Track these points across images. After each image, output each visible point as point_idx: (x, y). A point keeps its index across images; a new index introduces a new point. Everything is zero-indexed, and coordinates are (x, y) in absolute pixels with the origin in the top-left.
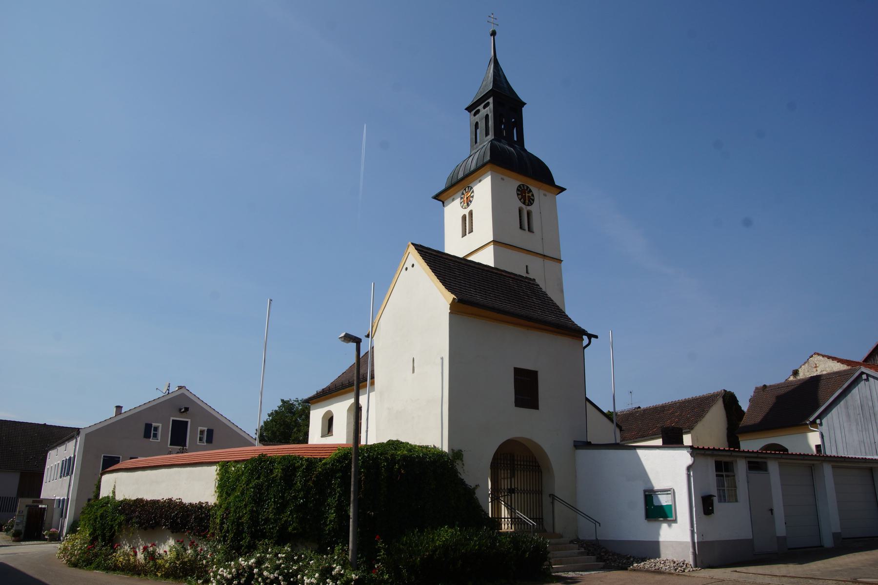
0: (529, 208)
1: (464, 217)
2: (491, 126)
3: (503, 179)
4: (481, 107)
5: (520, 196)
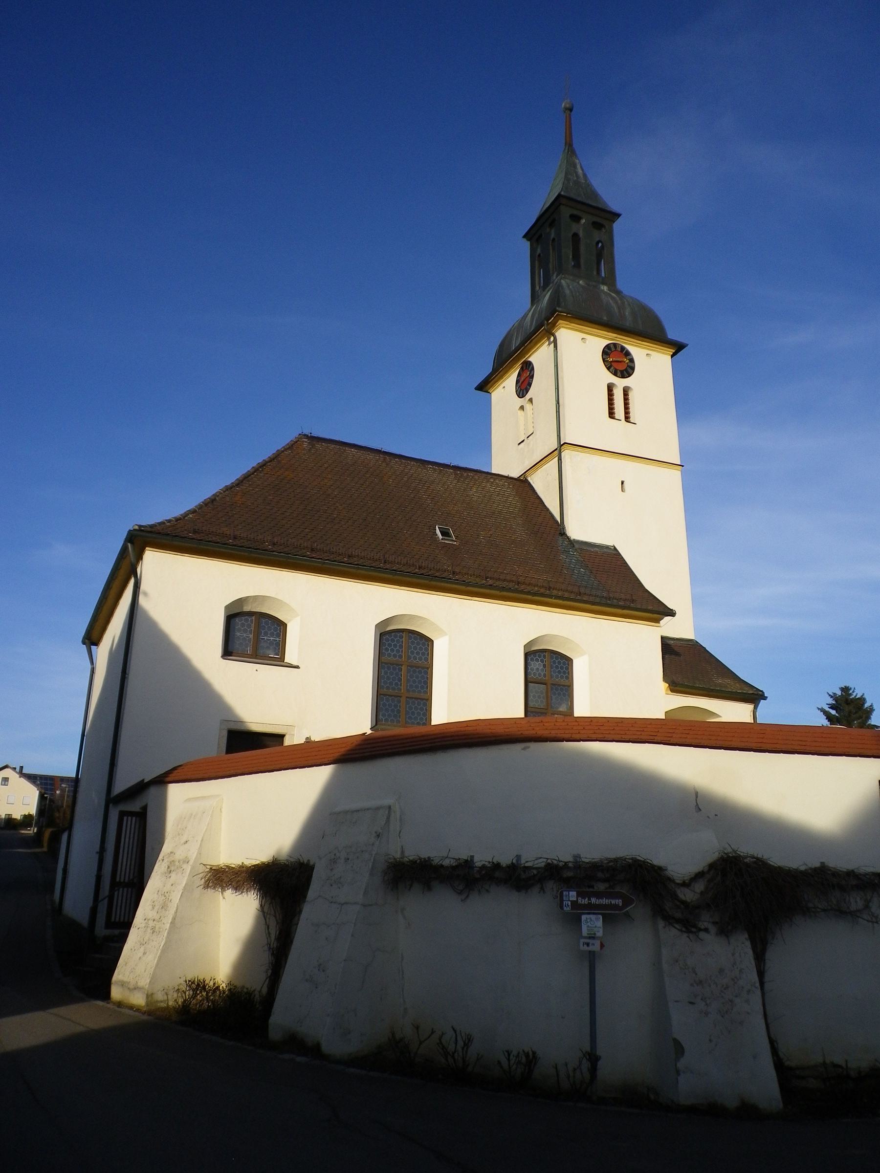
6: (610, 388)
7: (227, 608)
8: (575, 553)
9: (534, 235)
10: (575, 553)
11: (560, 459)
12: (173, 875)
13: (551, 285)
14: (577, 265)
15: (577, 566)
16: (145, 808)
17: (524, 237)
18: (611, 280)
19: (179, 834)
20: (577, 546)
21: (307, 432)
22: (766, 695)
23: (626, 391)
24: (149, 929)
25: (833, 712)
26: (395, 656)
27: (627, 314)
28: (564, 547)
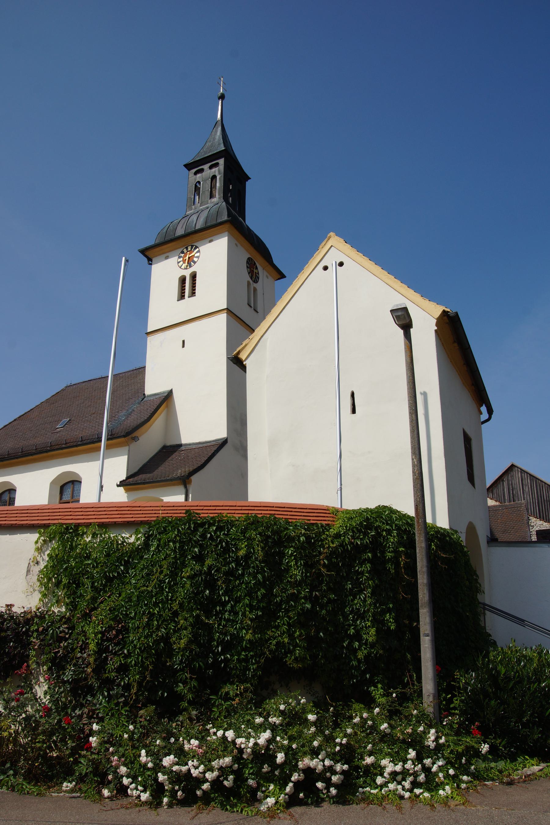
0: (255, 285)
1: (183, 280)
2: (219, 189)
3: (236, 245)
4: (206, 167)
5: (249, 269)
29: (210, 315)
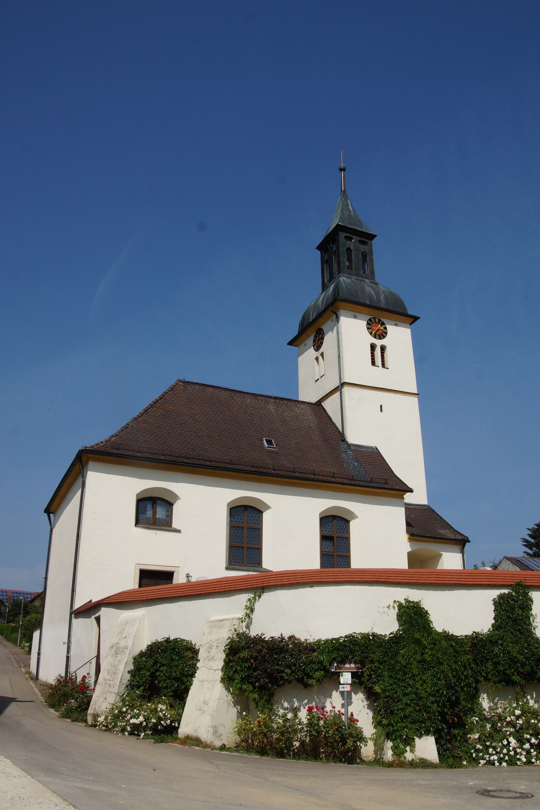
6: (373, 347)
7: (137, 495)
8: (351, 453)
9: (323, 247)
10: (351, 453)
11: (341, 393)
12: (119, 656)
13: (334, 280)
14: (350, 267)
15: (352, 461)
16: (99, 616)
17: (316, 248)
18: (372, 276)
19: (121, 633)
20: (352, 448)
21: (181, 379)
22: (469, 540)
23: (383, 348)
24: (107, 685)
25: (532, 541)
26: (239, 522)
27: (382, 298)
28: (344, 449)
29: (405, 394)
